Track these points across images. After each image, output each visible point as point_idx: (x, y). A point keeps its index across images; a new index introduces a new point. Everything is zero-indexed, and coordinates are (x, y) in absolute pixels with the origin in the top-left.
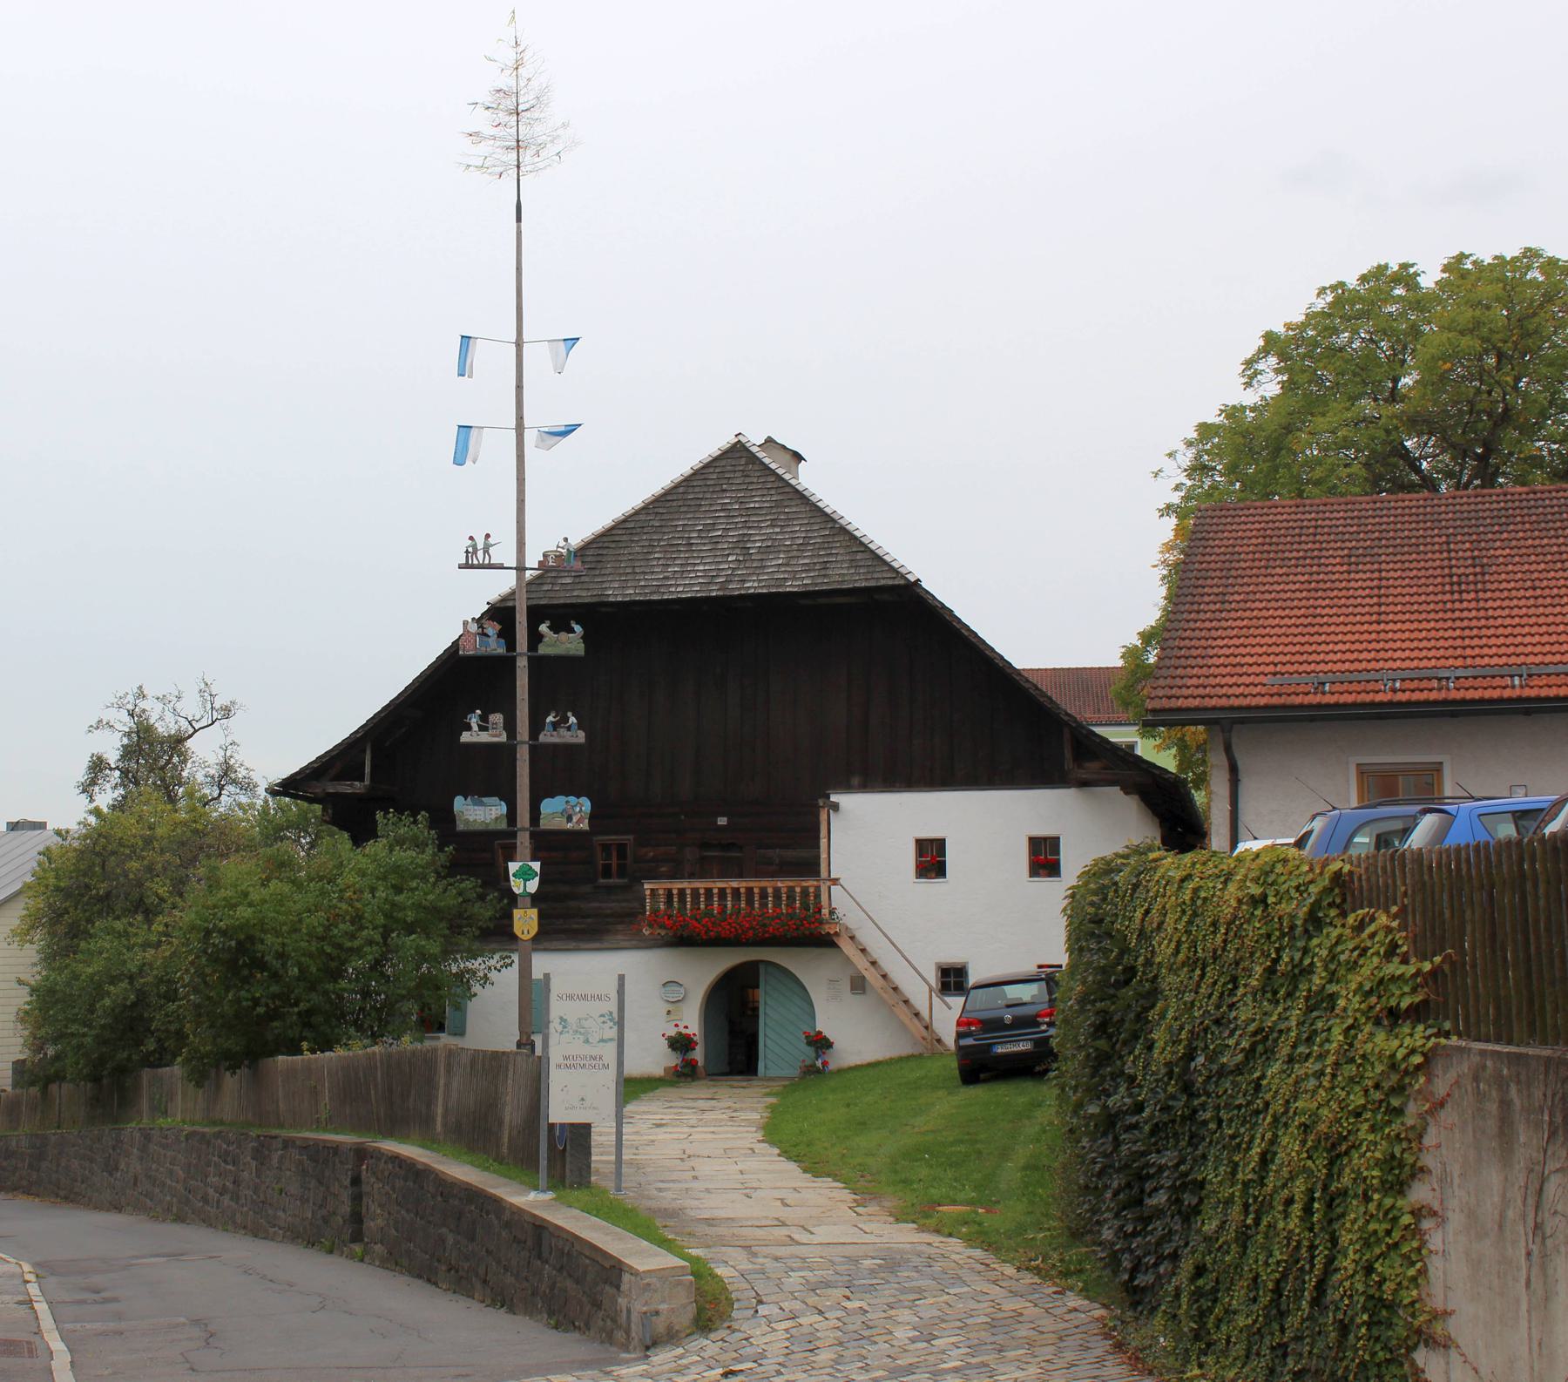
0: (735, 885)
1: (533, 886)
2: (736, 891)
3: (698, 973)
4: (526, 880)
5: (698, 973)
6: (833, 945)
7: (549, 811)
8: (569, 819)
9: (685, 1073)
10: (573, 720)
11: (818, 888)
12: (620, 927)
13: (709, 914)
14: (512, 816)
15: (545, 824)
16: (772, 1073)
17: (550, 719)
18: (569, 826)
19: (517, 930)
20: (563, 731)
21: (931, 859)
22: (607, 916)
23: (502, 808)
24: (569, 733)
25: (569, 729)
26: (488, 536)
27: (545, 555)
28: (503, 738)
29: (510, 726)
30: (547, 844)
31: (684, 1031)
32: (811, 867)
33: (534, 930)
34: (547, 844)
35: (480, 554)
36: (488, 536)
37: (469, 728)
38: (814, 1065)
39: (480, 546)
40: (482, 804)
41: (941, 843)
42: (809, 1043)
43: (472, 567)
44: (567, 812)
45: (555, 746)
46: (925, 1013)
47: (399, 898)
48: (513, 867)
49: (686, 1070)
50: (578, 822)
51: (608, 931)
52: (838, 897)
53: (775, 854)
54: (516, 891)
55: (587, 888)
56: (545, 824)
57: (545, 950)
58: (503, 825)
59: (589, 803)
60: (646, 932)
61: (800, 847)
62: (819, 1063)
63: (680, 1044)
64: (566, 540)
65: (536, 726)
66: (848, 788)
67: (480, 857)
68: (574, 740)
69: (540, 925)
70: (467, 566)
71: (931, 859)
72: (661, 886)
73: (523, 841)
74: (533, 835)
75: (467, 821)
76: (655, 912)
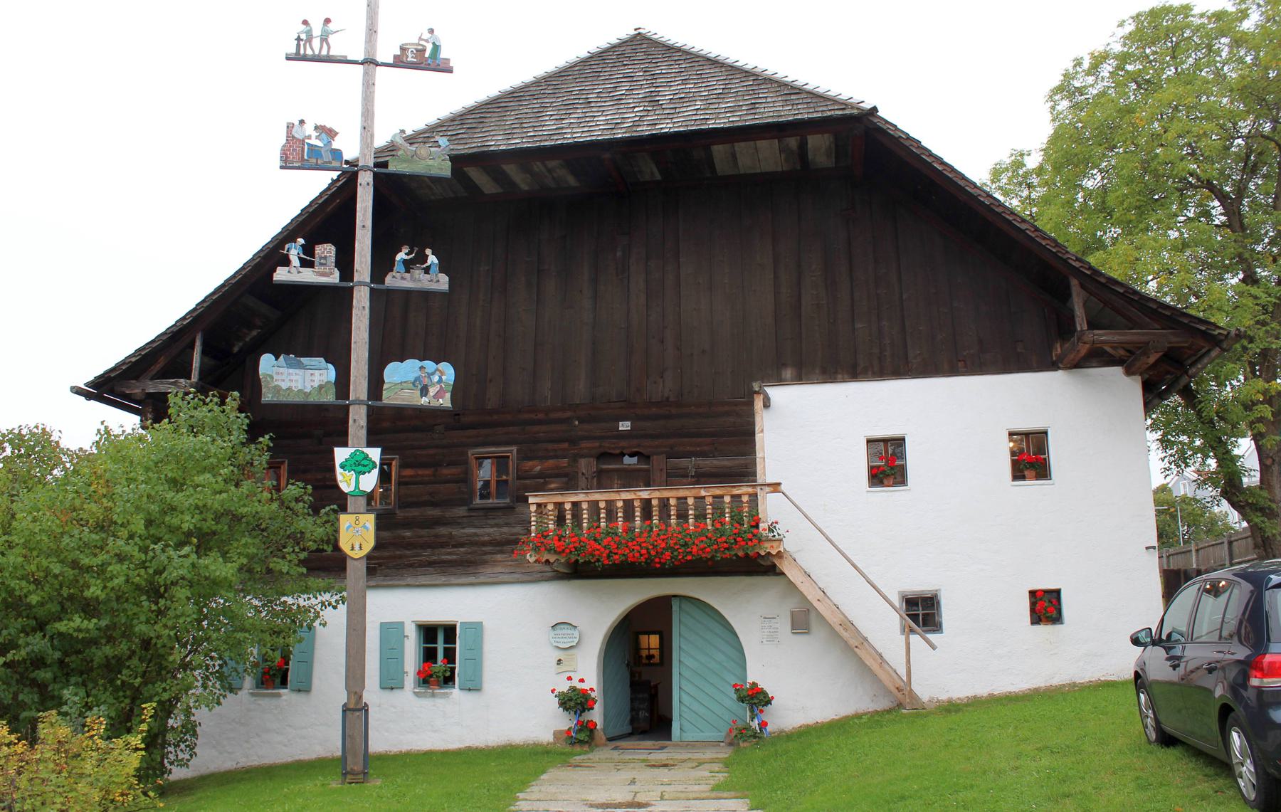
0: (645, 495)
3: (597, 612)
5: (597, 612)
7: (397, 379)
8: (424, 391)
9: (582, 738)
10: (432, 259)
12: (499, 557)
13: (611, 533)
14: (342, 384)
15: (391, 397)
16: (689, 736)
17: (401, 256)
18: (424, 401)
20: (418, 273)
21: (887, 463)
22: (484, 544)
23: (330, 373)
24: (431, 278)
25: (427, 270)
26: (327, 21)
27: (403, 49)
28: (334, 278)
29: (345, 263)
30: (390, 426)
31: (580, 686)
32: (746, 473)
33: (370, 543)
34: (390, 426)
35: (316, 43)
36: (327, 21)
37: (286, 262)
38: (748, 728)
39: (317, 31)
40: (302, 367)
41: (900, 442)
42: (741, 700)
43: (305, 58)
44: (421, 382)
45: (407, 293)
47: (178, 498)
48: (341, 454)
49: (582, 736)
50: (437, 396)
51: (485, 562)
52: (772, 508)
53: (691, 463)
54: (345, 488)
55: (461, 511)
57: (408, 586)
58: (330, 397)
59: (452, 371)
60: (531, 557)
61: (727, 446)
62: (755, 724)
63: (575, 702)
64: (431, 31)
65: (382, 264)
66: (780, 381)
67: (300, 440)
68: (434, 287)
69: (377, 538)
70: (297, 57)
71: (887, 463)
72: (549, 499)
73: (358, 419)
75: (278, 389)
76: (543, 534)
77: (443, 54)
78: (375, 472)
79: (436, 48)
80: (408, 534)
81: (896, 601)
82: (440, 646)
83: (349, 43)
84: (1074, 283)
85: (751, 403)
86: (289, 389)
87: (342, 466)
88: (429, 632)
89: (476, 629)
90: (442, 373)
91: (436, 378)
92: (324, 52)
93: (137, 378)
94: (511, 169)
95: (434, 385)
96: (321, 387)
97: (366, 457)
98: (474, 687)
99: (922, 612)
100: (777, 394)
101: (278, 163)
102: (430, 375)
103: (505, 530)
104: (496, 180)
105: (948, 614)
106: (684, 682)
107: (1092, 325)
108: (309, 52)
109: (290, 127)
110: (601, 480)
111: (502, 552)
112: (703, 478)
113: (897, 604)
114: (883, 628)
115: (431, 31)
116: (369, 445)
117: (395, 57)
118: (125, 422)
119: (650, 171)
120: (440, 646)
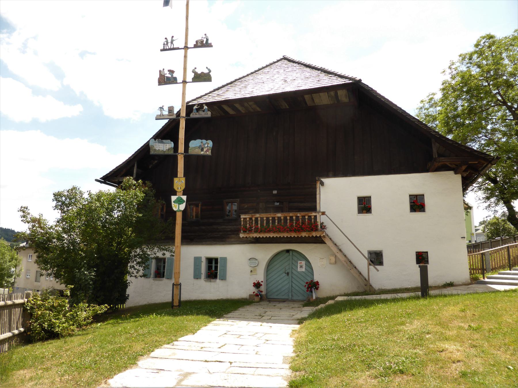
1: (182, 207)
2: (279, 218)
4: (179, 204)
6: (323, 242)
7: (193, 146)
8: (202, 150)
11: (316, 216)
12: (233, 236)
15: (191, 152)
18: (202, 153)
19: (175, 187)
20: (201, 112)
21: (365, 205)
25: (204, 111)
26: (173, 37)
35: (169, 44)
36: (173, 37)
39: (169, 41)
43: (166, 50)
46: (367, 279)
48: (174, 198)
50: (206, 151)
54: (175, 209)
56: (191, 152)
58: (172, 152)
59: (212, 143)
61: (310, 201)
64: (205, 35)
66: (327, 176)
68: (206, 116)
70: (164, 50)
71: (365, 205)
74: (185, 157)
75: (155, 150)
77: (209, 42)
78: (185, 204)
79: (207, 40)
80: (204, 228)
81: (366, 255)
82: (213, 265)
83: (179, 43)
84: (433, 140)
85: (316, 183)
86: (159, 150)
87: (174, 202)
88: (210, 260)
89: (225, 259)
90: (208, 144)
91: (206, 145)
92: (172, 47)
93: (116, 176)
94: (237, 105)
95: (205, 147)
96: (169, 149)
97: (182, 199)
98: (224, 278)
99: (376, 258)
100: (325, 180)
101: (157, 83)
102: (204, 144)
103: (235, 227)
104: (233, 109)
105: (386, 259)
106: (293, 279)
107: (440, 155)
108: (167, 48)
109: (160, 71)
110: (266, 211)
111: (234, 234)
112: (300, 210)
113: (367, 256)
114: (362, 264)
115: (205, 35)
116: (183, 195)
117: (194, 45)
118: (111, 189)
119: (285, 105)
120: (213, 265)
